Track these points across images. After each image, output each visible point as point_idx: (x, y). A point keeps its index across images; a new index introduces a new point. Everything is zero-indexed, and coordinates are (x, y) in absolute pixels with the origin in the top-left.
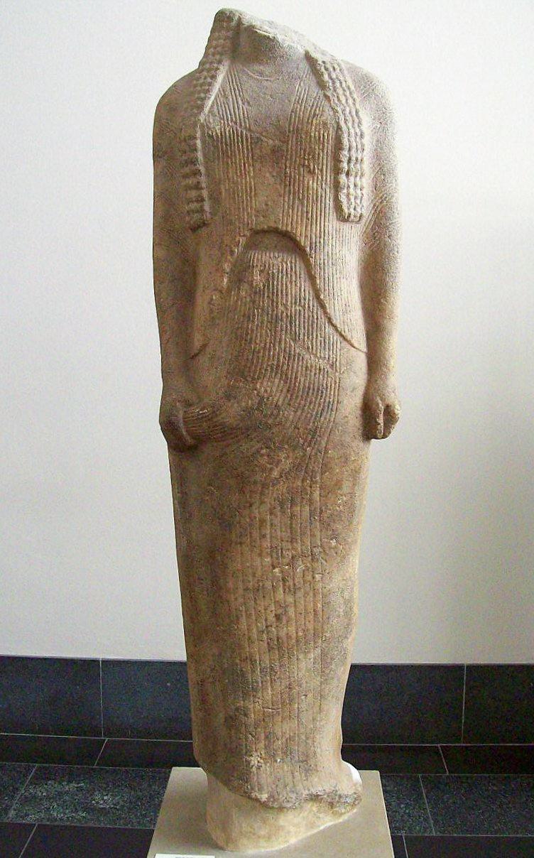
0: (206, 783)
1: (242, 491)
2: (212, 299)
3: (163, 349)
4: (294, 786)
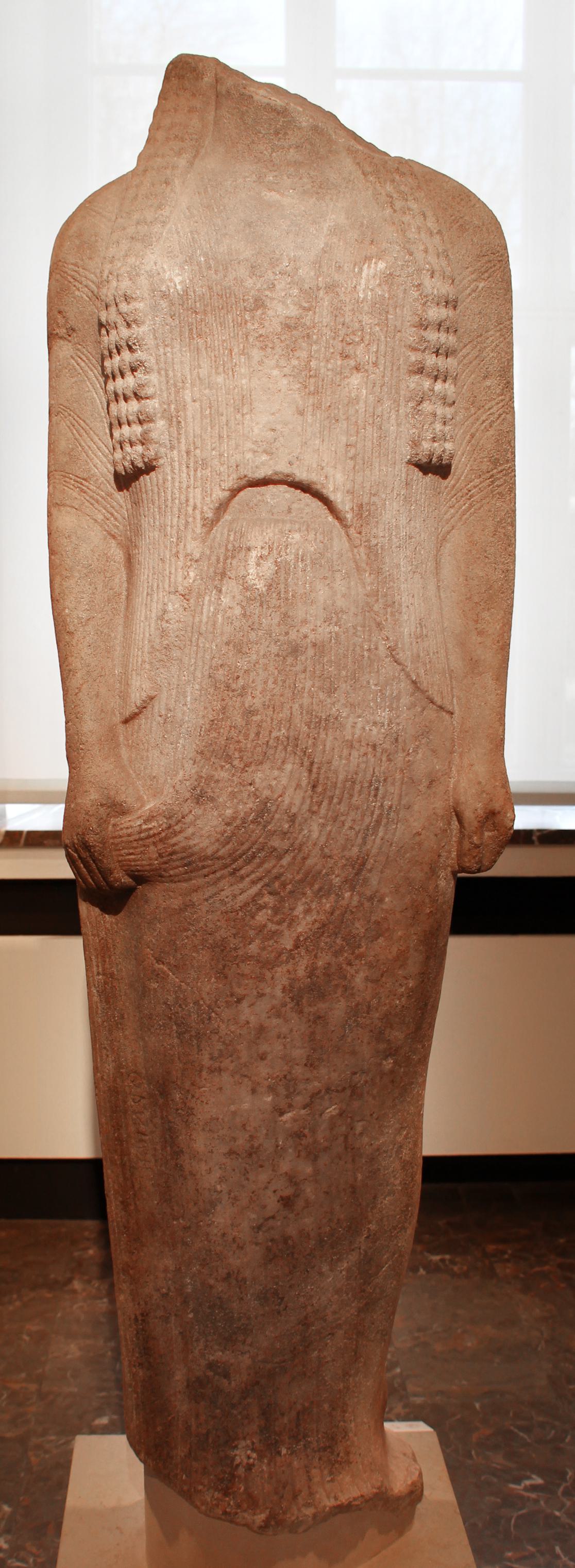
0: (66, 788)
1: (222, 975)
2: (165, 611)
3: (410, 163)
4: (311, 1494)
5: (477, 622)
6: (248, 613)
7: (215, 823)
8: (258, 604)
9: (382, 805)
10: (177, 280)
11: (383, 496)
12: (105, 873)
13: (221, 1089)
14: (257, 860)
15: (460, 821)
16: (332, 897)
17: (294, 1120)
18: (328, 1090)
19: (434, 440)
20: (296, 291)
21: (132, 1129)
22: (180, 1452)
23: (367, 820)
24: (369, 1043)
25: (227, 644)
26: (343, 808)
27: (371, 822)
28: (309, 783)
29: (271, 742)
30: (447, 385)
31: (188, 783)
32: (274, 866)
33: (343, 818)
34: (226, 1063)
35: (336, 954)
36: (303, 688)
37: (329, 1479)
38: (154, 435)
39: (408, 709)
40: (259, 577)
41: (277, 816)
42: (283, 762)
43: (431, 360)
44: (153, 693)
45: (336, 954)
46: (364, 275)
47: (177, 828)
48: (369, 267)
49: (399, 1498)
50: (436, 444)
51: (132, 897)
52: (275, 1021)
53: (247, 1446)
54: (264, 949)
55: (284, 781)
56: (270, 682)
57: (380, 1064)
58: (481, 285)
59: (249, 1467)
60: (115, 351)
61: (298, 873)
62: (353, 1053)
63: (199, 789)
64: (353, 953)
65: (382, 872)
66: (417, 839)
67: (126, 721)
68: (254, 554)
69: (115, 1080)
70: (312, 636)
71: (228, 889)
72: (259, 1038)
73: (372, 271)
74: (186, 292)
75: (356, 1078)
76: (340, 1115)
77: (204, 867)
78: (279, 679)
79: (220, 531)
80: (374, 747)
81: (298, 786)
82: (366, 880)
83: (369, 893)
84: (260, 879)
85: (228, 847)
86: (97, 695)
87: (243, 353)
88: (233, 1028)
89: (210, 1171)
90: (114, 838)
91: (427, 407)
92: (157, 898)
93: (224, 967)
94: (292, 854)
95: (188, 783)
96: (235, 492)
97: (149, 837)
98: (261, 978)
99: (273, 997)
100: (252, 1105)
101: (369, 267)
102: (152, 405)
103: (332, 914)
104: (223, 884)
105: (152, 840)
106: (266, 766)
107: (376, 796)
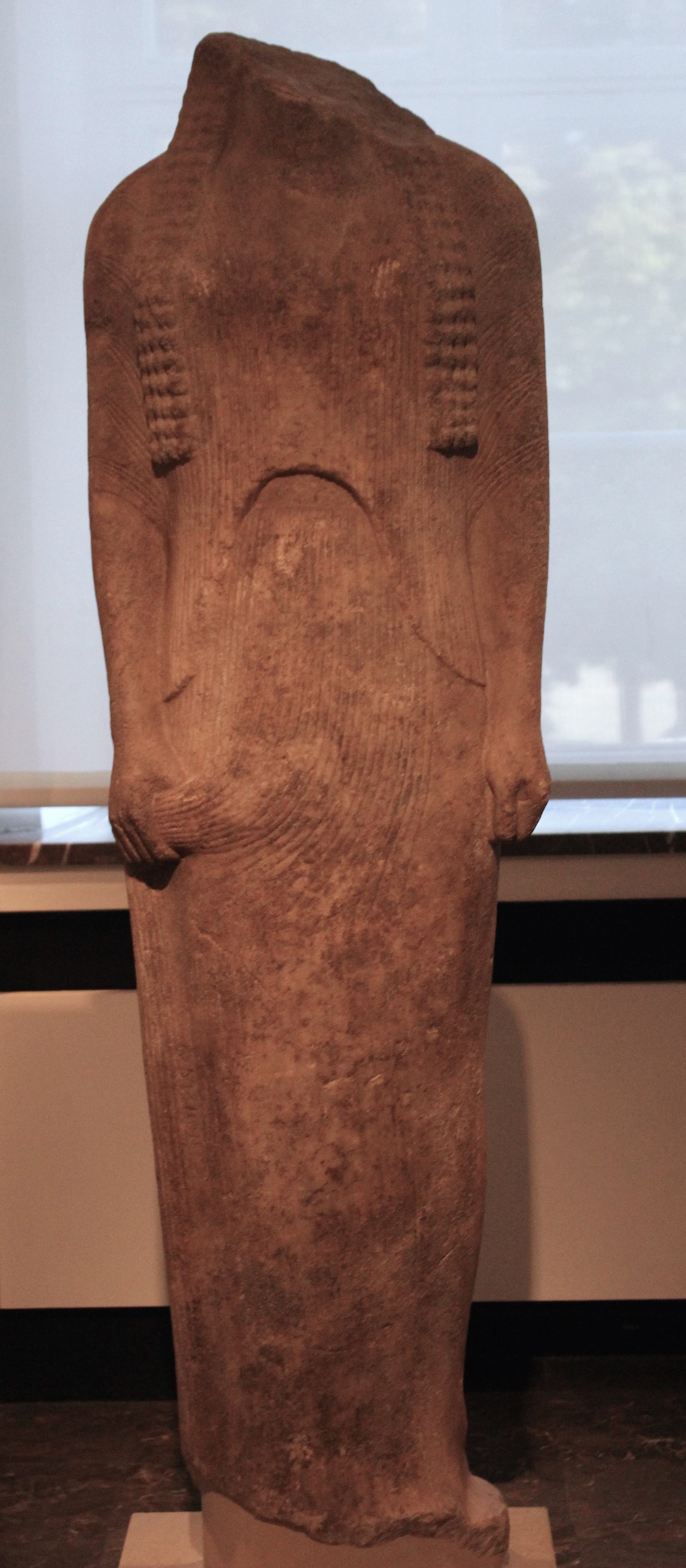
1: (263, 942)
2: (201, 596)
4: (374, 1503)
5: (506, 596)
6: (278, 597)
7: (252, 795)
8: (287, 589)
9: (411, 777)
10: (205, 284)
11: (405, 482)
12: (150, 846)
13: (265, 1056)
14: (292, 830)
15: (492, 789)
16: (367, 864)
17: (339, 1088)
18: (371, 1058)
19: (454, 425)
20: (316, 293)
21: (181, 1104)
22: (234, 1451)
23: (397, 790)
24: (411, 1012)
25: (259, 626)
26: (373, 779)
27: (400, 793)
28: (339, 756)
29: (302, 718)
30: (467, 371)
31: (225, 758)
32: (310, 835)
33: (373, 789)
34: (269, 1030)
35: (372, 920)
36: (331, 667)
37: (393, 1490)
38: (187, 430)
39: (435, 683)
40: (287, 562)
41: (310, 788)
42: (314, 737)
43: (447, 351)
44: (191, 673)
45: (372, 920)
46: (379, 275)
47: (216, 800)
48: (384, 267)
49: (477, 1532)
50: (457, 429)
51: (176, 872)
52: (315, 987)
53: (303, 1441)
54: (302, 916)
55: (316, 754)
56: (300, 661)
57: (425, 1033)
58: (503, 267)
59: (306, 1465)
60: (148, 348)
61: (332, 841)
62: (396, 1021)
63: (235, 763)
64: (389, 920)
65: (414, 840)
66: (448, 808)
67: (168, 700)
68: (282, 541)
69: (163, 1055)
70: (338, 618)
71: (266, 858)
72: (300, 1004)
73: (387, 271)
74: (213, 294)
75: (400, 1047)
76: (386, 1084)
77: (242, 838)
78: (308, 658)
79: (250, 520)
80: (401, 720)
81: (329, 759)
82: (399, 849)
83: (402, 861)
84: (296, 848)
85: (266, 817)
86: (140, 676)
87: (268, 352)
88: (275, 994)
89: (257, 1141)
90: (157, 811)
91: (446, 395)
92: (200, 870)
93: (265, 933)
94: (326, 824)
95: (225, 758)
96: (263, 483)
97: (190, 810)
98: (300, 945)
99: (312, 963)
100: (297, 1072)
101: (384, 267)
102: (185, 401)
103: (367, 881)
104: (262, 853)
105: (192, 812)
106: (299, 740)
107: (405, 766)
